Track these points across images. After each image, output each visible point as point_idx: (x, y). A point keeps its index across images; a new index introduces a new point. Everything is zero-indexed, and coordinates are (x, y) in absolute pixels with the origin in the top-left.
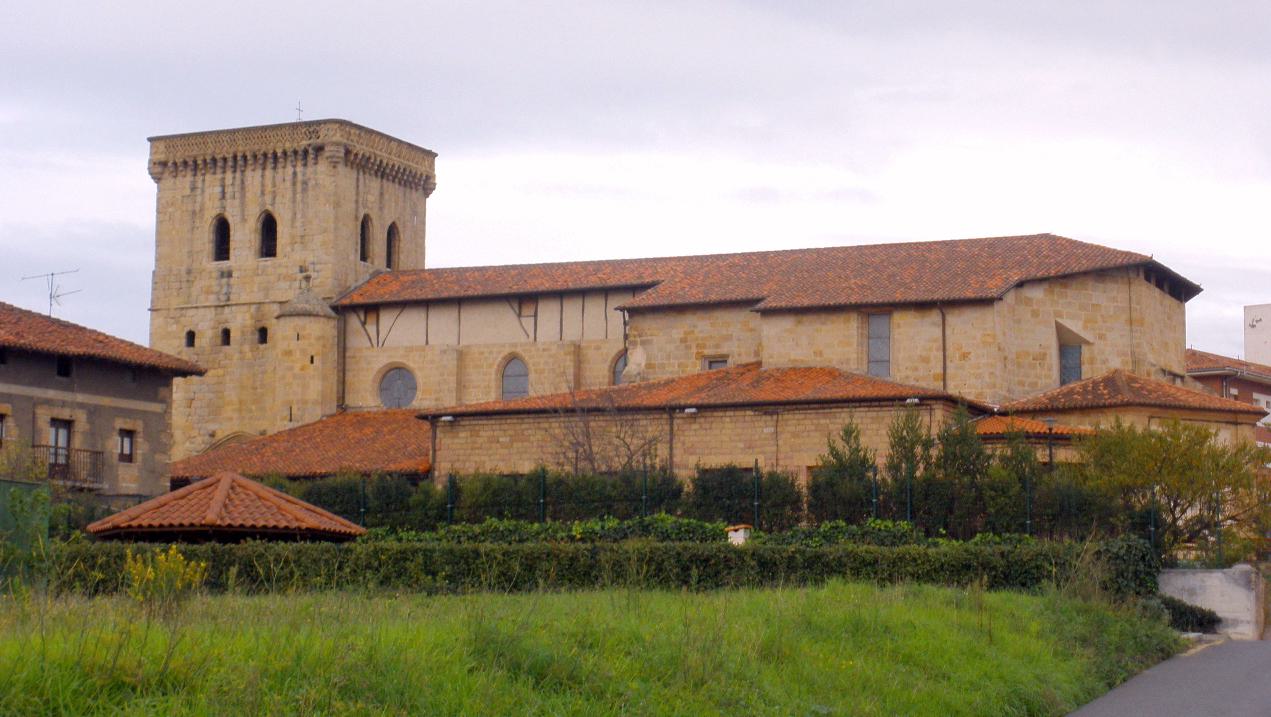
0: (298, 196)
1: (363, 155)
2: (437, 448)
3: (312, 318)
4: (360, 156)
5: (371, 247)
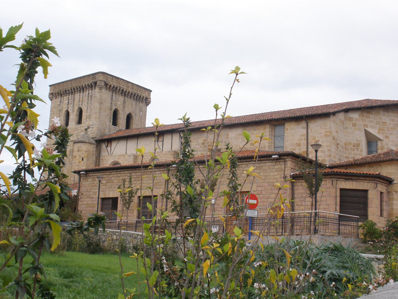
0: (89, 101)
1: (114, 86)
2: (80, 186)
3: (84, 144)
4: (112, 86)
5: (118, 121)
